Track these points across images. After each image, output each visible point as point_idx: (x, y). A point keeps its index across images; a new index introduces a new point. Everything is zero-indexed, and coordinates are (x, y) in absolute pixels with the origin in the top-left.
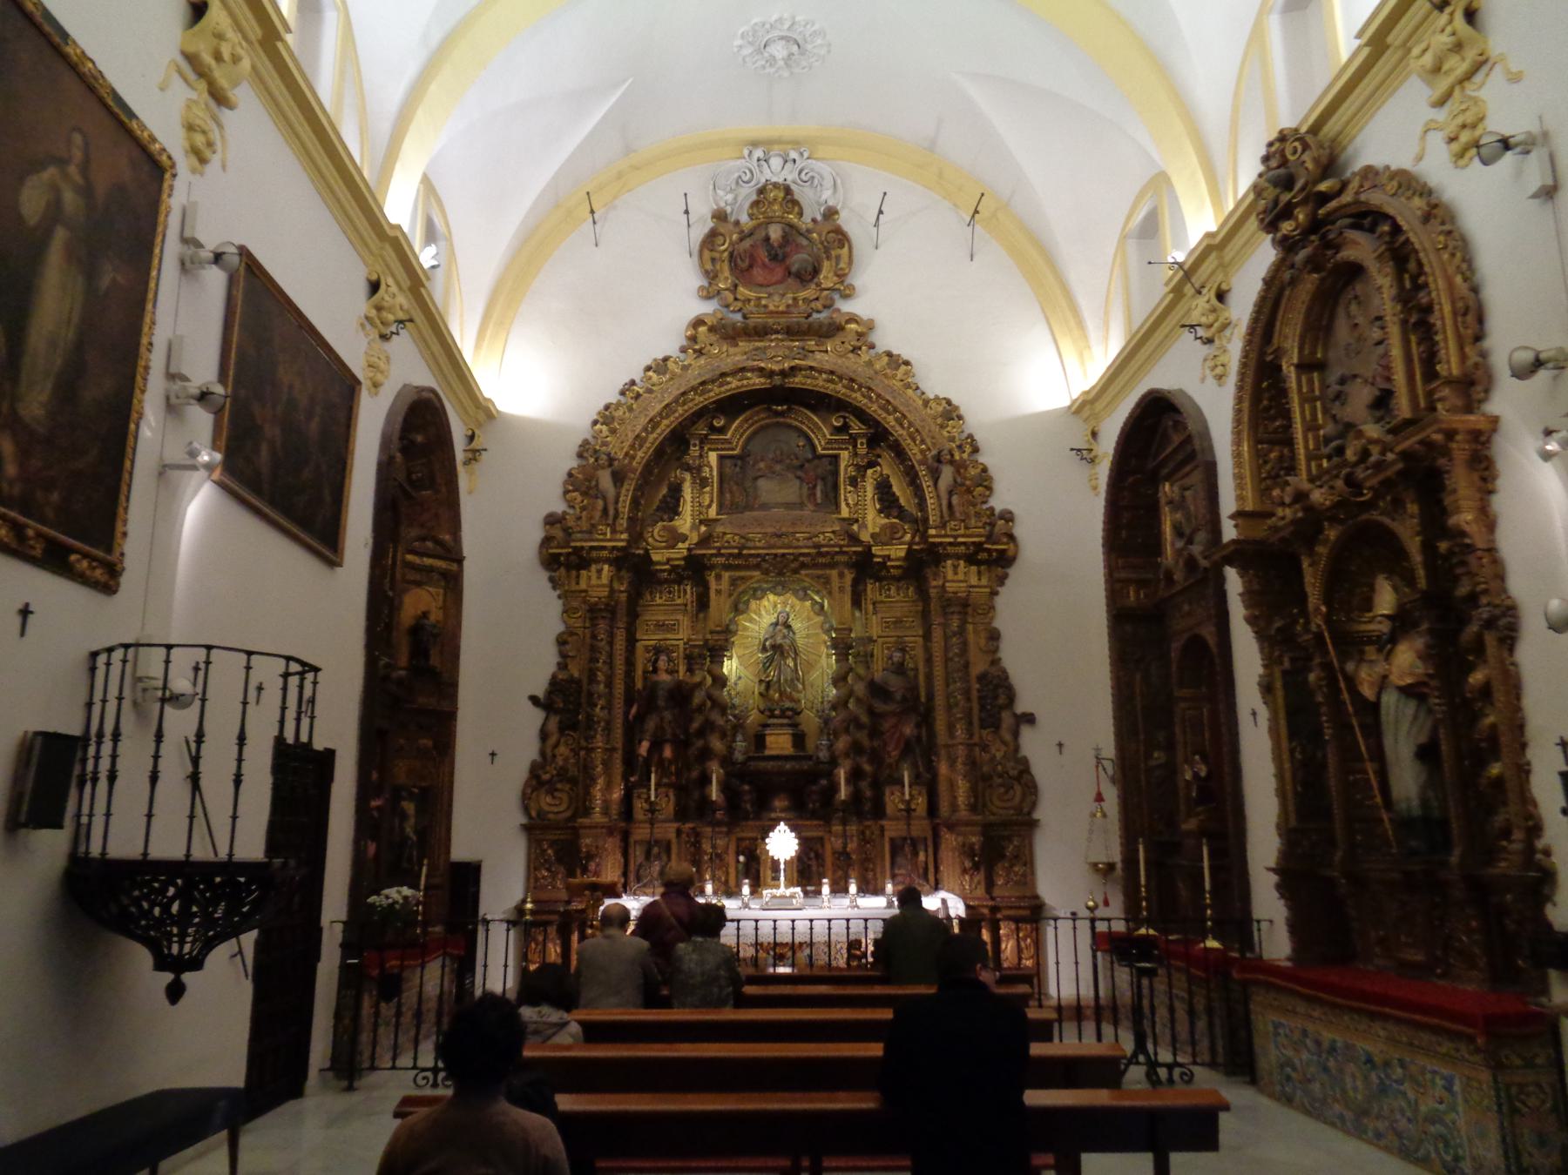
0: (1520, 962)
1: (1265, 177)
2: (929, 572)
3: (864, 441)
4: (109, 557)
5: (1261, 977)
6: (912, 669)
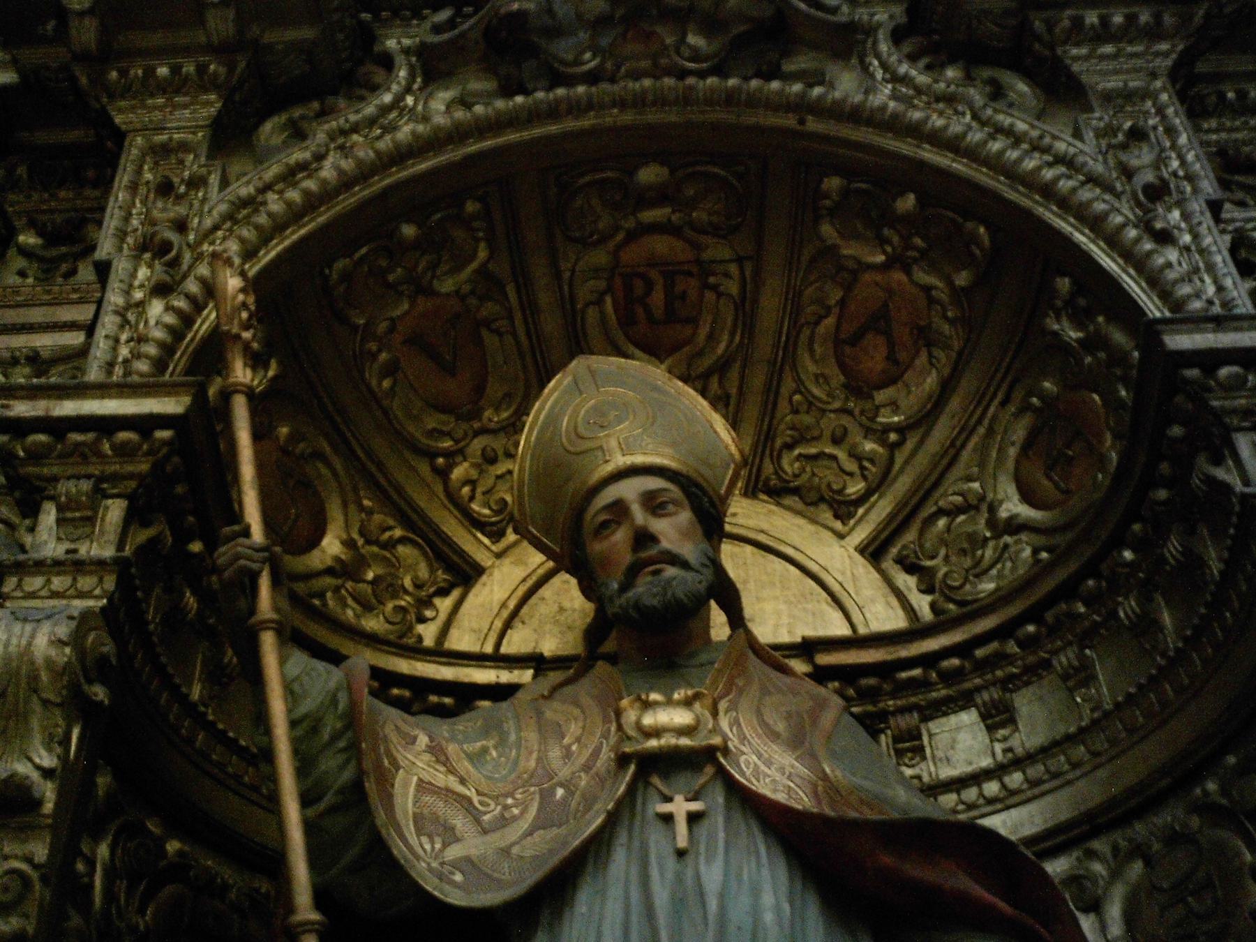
1: (666, 791)
2: (903, 20)
3: (160, 204)
4: (123, 554)
5: (966, 305)
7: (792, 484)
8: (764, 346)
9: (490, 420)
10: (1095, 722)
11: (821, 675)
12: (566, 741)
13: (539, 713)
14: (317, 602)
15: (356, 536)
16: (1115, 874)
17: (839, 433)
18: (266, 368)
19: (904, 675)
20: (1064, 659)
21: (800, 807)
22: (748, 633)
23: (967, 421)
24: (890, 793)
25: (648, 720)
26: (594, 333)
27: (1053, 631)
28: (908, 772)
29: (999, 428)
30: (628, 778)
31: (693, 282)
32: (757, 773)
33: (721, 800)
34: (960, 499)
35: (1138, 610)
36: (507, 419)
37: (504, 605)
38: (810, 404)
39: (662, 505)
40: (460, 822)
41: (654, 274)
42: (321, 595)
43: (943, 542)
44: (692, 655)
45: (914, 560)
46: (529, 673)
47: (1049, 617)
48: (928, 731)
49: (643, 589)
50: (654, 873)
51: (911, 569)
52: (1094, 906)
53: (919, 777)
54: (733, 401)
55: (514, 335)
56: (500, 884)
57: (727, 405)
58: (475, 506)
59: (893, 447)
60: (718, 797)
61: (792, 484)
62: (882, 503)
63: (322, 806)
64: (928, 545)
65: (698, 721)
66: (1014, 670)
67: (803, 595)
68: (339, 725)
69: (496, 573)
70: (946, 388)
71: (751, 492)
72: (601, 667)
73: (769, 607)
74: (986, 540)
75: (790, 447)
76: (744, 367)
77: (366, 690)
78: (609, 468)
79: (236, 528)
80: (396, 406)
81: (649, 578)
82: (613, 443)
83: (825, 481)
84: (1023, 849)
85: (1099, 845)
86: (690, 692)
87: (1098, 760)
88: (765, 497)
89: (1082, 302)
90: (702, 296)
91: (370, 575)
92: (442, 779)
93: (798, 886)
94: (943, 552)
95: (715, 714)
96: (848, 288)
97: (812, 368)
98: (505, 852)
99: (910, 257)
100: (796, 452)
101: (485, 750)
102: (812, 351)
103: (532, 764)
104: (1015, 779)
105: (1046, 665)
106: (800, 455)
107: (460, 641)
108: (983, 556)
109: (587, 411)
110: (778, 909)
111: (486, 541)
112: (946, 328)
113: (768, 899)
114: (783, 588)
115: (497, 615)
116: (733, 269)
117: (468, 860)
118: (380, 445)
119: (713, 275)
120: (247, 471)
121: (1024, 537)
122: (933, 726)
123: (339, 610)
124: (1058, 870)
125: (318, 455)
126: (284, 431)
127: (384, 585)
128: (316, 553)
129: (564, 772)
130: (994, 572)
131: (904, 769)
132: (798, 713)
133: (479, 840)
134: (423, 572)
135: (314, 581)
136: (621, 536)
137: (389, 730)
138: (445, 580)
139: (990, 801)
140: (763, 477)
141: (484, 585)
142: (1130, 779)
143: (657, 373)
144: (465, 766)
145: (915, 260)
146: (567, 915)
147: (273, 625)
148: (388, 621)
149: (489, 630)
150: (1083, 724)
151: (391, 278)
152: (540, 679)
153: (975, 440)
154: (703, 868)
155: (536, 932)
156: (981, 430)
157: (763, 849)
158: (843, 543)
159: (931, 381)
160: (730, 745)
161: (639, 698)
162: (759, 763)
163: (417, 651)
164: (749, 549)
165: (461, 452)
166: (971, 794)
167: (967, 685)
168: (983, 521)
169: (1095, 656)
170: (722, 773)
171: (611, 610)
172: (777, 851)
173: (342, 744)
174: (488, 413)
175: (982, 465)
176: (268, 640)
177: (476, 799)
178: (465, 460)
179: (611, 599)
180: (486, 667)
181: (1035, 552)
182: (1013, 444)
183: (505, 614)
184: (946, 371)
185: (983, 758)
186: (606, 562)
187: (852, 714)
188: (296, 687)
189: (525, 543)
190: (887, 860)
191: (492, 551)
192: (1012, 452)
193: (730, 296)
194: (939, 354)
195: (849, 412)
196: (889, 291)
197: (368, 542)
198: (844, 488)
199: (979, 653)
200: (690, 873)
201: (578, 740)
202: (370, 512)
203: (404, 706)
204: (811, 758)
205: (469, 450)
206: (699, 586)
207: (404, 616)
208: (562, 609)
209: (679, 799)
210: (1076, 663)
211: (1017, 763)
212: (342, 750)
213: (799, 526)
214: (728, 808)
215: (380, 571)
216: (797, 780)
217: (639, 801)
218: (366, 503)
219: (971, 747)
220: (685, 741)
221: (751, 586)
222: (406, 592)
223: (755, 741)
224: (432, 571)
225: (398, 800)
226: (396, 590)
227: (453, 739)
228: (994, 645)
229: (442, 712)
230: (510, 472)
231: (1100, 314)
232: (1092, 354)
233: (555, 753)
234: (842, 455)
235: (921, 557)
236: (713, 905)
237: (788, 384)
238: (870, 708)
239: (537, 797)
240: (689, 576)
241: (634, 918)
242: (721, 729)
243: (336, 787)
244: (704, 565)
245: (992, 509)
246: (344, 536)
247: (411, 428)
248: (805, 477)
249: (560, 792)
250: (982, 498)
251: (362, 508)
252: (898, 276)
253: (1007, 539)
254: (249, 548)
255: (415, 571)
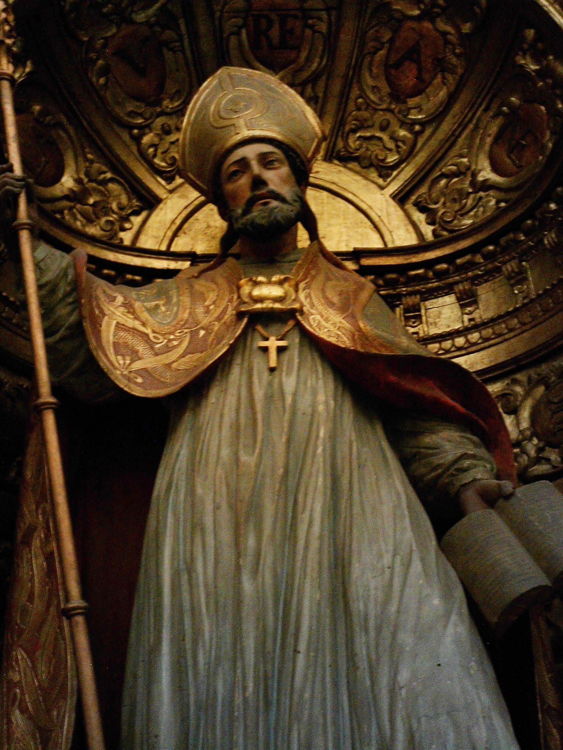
0: (541, 83)
6: (376, 93)
7: (353, 155)
8: (341, 67)
9: (167, 107)
10: (524, 305)
11: (363, 271)
12: (207, 303)
13: (191, 287)
14: (58, 216)
15: (83, 176)
16: (528, 394)
17: (385, 123)
18: (24, 66)
19: (413, 273)
20: (509, 267)
21: (343, 346)
22: (321, 245)
23: (463, 120)
24: (397, 339)
25: (256, 292)
26: (234, 53)
27: (505, 250)
28: (412, 330)
29: (482, 125)
30: (242, 326)
31: (298, 23)
32: (319, 325)
33: (297, 340)
34: (454, 168)
35: (556, 240)
36: (178, 106)
37: (173, 222)
38: (368, 105)
39: (271, 162)
40: (141, 348)
41: (274, 16)
42: (61, 212)
43: (443, 194)
44: (285, 256)
45: (425, 205)
46: (187, 264)
47: (503, 241)
48: (425, 307)
49: (256, 213)
50: (256, 381)
51: (422, 209)
52: (514, 411)
53: (417, 333)
54: (320, 100)
55: (183, 51)
56: (164, 385)
57: (316, 103)
58: (156, 161)
59: (417, 134)
60: (295, 338)
61: (353, 155)
62: (408, 169)
63: (58, 336)
64: (434, 195)
65: (286, 293)
66: (480, 273)
67: (356, 224)
68: (68, 289)
69: (169, 202)
70: (452, 98)
71: (328, 158)
72: (231, 261)
73: (335, 229)
74: (469, 193)
75: (354, 131)
76: (328, 79)
77: (85, 268)
78: (238, 138)
79: (4, 166)
80: (108, 95)
81: (261, 207)
82: (242, 122)
83: (375, 153)
84: (474, 376)
85: (521, 376)
86: (282, 277)
87: (524, 328)
88: (336, 162)
89: (540, 45)
90: (303, 32)
91: (91, 201)
92: (131, 322)
93: (340, 388)
94: (442, 200)
95: (297, 291)
96: (395, 31)
97: (370, 81)
98: (169, 365)
99: (435, 12)
100: (358, 135)
101: (157, 307)
102: (371, 71)
103: (186, 316)
104: (475, 337)
105: (498, 270)
106: (360, 137)
107: (146, 242)
108: (466, 203)
109: (227, 101)
110: (326, 403)
111: (163, 182)
112: (454, 60)
113: (321, 398)
114: (345, 218)
115: (169, 228)
116: (324, 15)
117: (145, 370)
118: (98, 122)
119: (310, 19)
120: (11, 130)
121: (491, 193)
122: (428, 304)
123: (72, 221)
124: (496, 390)
125: (59, 125)
126: (37, 108)
127: (100, 207)
128: (58, 186)
129: (205, 321)
130: (472, 213)
131: (408, 328)
132: (347, 291)
133: (153, 359)
134: (124, 199)
135: (56, 203)
136: (244, 181)
137: (99, 293)
138: (137, 206)
139: (459, 349)
140: (336, 150)
141: (162, 209)
142: (541, 339)
143: (272, 80)
144: (145, 316)
145: (438, 15)
146: (203, 404)
147: (26, 227)
148: (102, 229)
149: (164, 236)
150: (518, 306)
151: (105, 10)
152: (192, 267)
153: (467, 132)
154: (284, 379)
155: (185, 413)
156: (471, 126)
157: (320, 369)
158: (383, 192)
159: (442, 94)
160: (305, 309)
161: (251, 280)
162: (322, 320)
163: (121, 248)
164: (325, 194)
165: (149, 126)
166: (447, 344)
167: (451, 280)
168: (468, 182)
169: (528, 266)
170: (298, 324)
171: (238, 225)
172: (329, 370)
173: (70, 300)
174: (165, 103)
175: (470, 147)
176: (25, 236)
177: (151, 335)
178: (151, 131)
179: (237, 220)
180: (162, 259)
181: (498, 202)
182: (489, 135)
183: (174, 228)
184: (452, 88)
185: (456, 323)
186: (234, 196)
187: (381, 296)
188: (42, 264)
189: (187, 186)
190: (393, 378)
191: (166, 189)
192: (489, 140)
193: (320, 32)
194: (450, 78)
195: (392, 111)
196: (422, 36)
197: (90, 181)
198: (385, 159)
199: (459, 261)
200: (276, 380)
201: (214, 303)
202: (92, 162)
203: (111, 280)
204: (352, 317)
205: (153, 125)
206: (292, 213)
207: (112, 226)
208: (208, 227)
209: (272, 339)
210: (516, 270)
211: (476, 327)
212: (70, 304)
213: (356, 180)
214: (301, 345)
215: (98, 198)
216: (343, 331)
217: (249, 339)
218: (90, 156)
219: (450, 317)
220: (277, 306)
221: (325, 216)
222: (113, 212)
223: (320, 307)
224: (130, 200)
225: (104, 334)
226: (108, 211)
227: (138, 299)
228: (468, 257)
229: (133, 284)
230: (178, 140)
231: (552, 55)
232: (543, 81)
233: (200, 310)
234: (385, 137)
235: (429, 202)
236: (289, 400)
237: (355, 92)
238: (391, 292)
239: (188, 335)
240: (285, 207)
241: (243, 406)
242: (299, 300)
243: (67, 324)
244: (295, 201)
245: (474, 175)
246: (76, 176)
247: (118, 110)
248: (363, 150)
249: (202, 333)
250: (468, 168)
251: (86, 160)
252: (427, 25)
253: (482, 194)
254: (12, 178)
255: (119, 199)
